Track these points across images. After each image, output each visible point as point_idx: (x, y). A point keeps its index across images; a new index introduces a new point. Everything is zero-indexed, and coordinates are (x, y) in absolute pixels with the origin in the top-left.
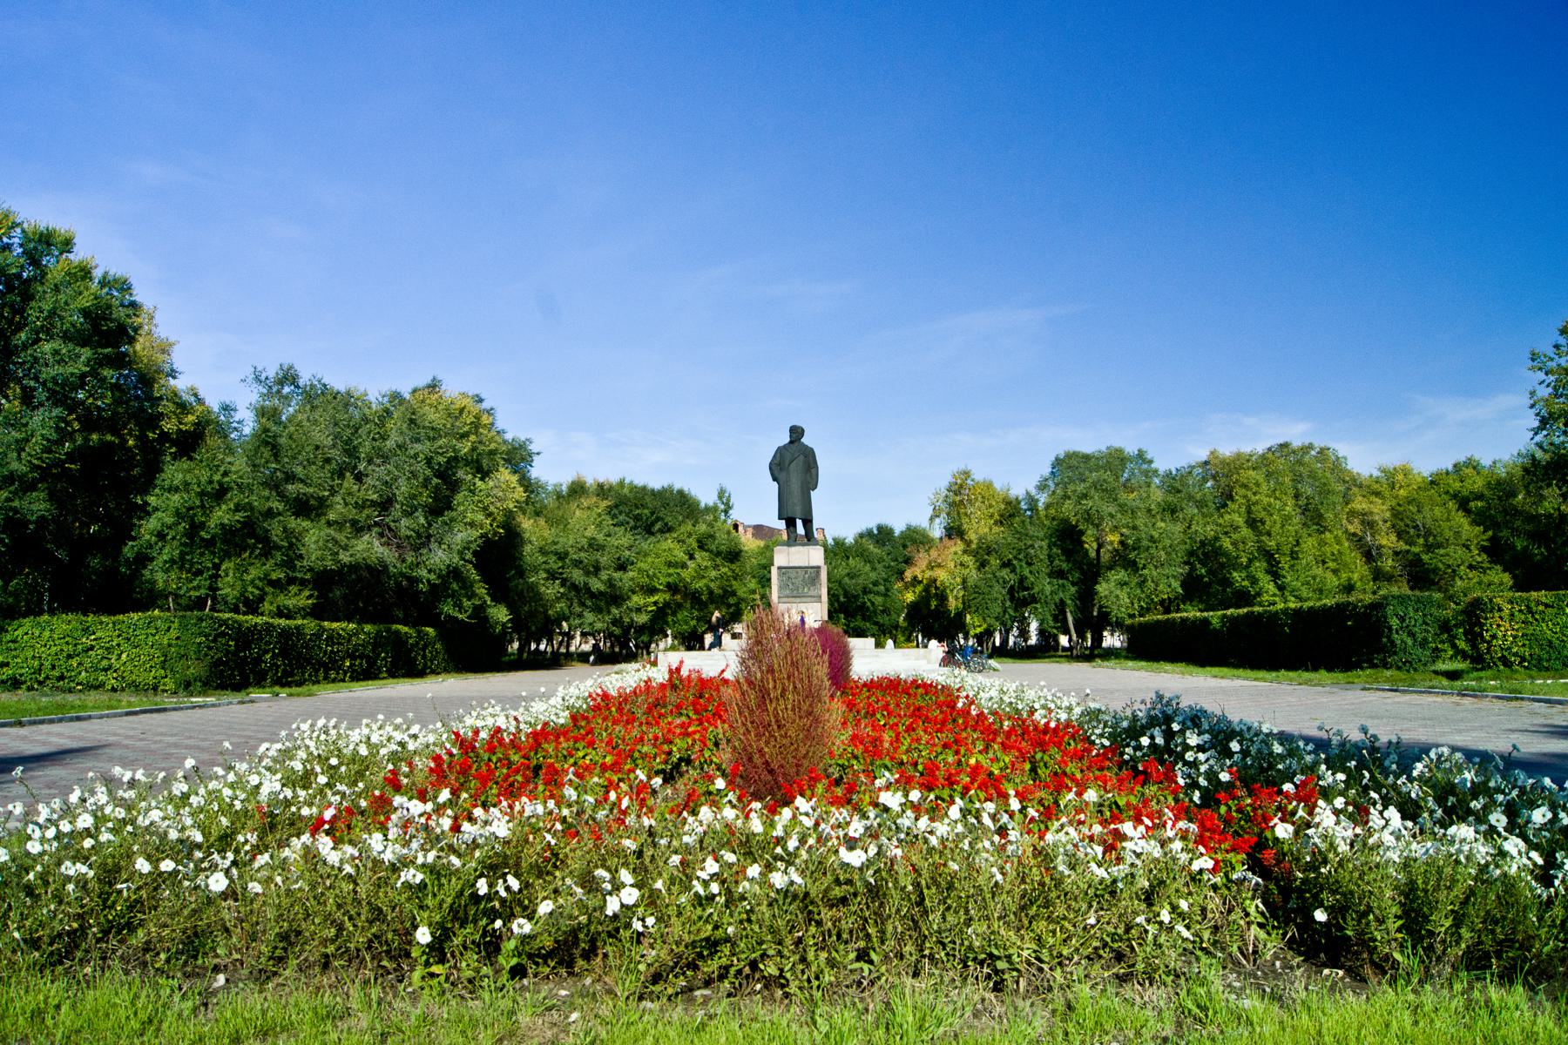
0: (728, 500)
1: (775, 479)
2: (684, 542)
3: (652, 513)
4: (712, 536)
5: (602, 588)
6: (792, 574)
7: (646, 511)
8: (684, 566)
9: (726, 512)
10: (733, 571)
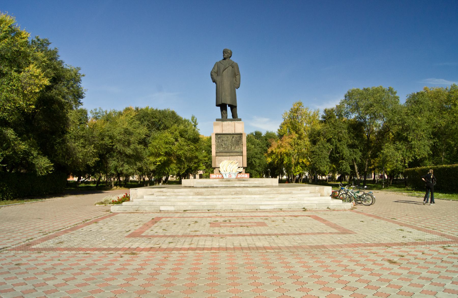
0: (196, 121)
1: (214, 81)
2: (173, 133)
3: (159, 120)
4: (186, 131)
5: (131, 153)
6: (225, 138)
7: (157, 120)
8: (173, 144)
9: (195, 126)
10: (195, 147)
